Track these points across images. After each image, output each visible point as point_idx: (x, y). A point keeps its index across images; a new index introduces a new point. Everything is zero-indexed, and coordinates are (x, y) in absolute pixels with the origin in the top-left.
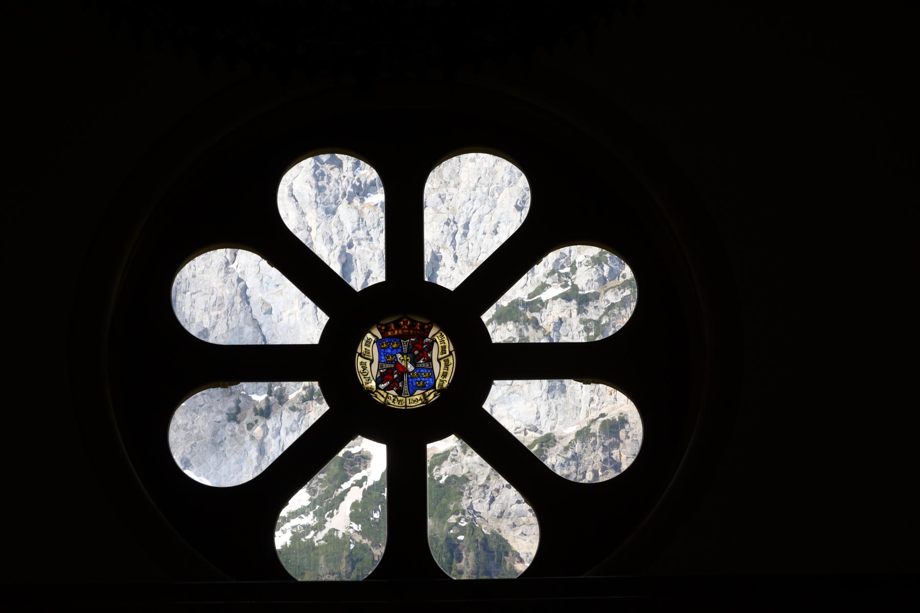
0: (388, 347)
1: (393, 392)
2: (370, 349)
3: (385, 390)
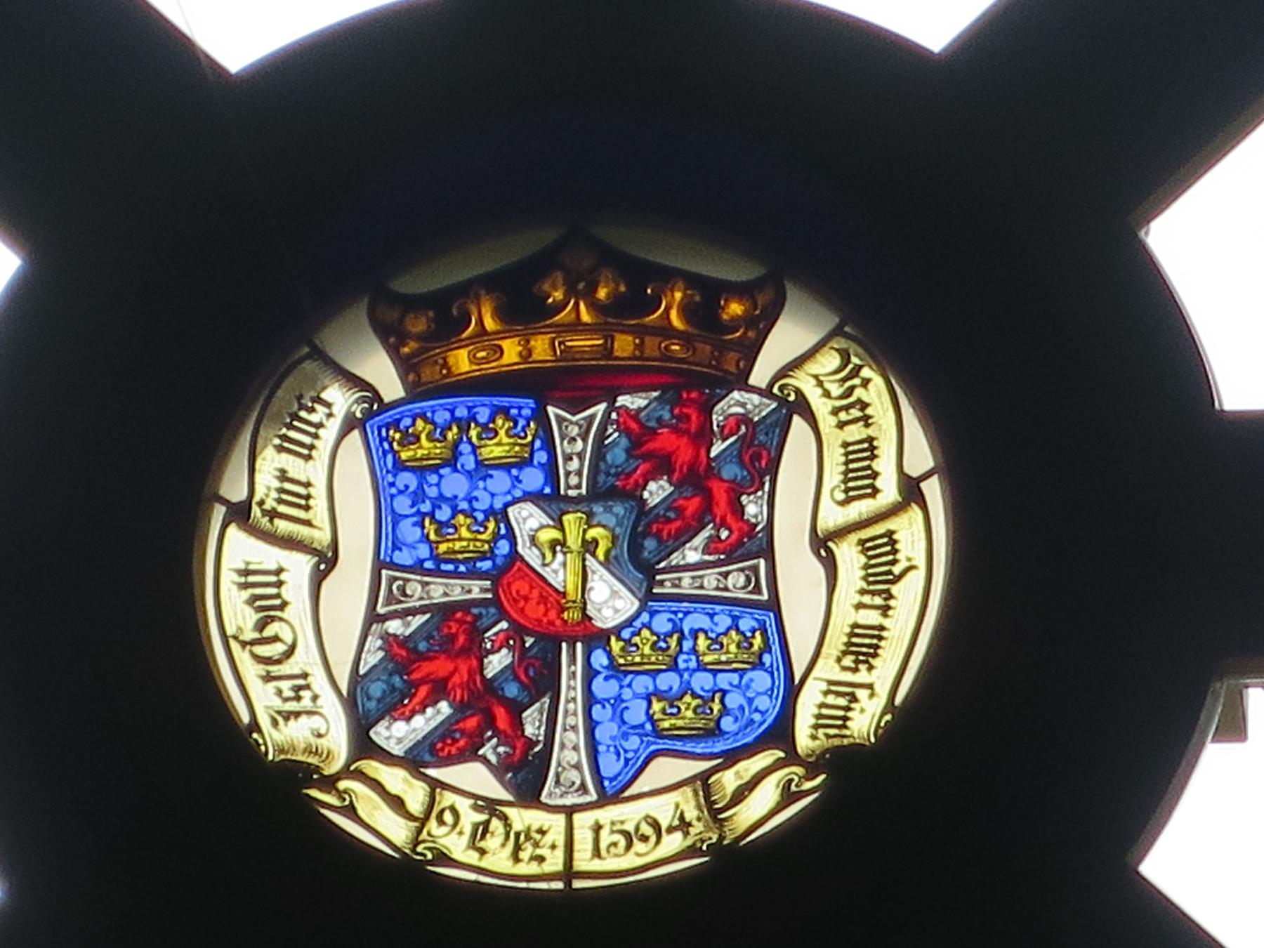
0: (452, 461)
1: (475, 777)
2: (315, 471)
3: (414, 761)
